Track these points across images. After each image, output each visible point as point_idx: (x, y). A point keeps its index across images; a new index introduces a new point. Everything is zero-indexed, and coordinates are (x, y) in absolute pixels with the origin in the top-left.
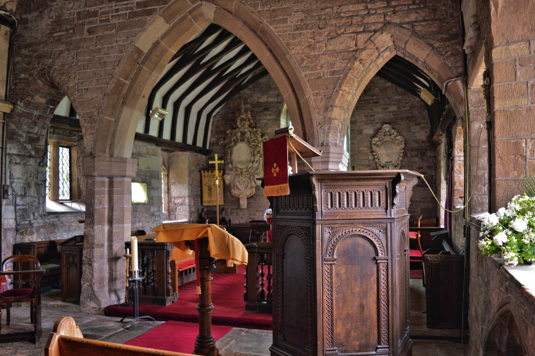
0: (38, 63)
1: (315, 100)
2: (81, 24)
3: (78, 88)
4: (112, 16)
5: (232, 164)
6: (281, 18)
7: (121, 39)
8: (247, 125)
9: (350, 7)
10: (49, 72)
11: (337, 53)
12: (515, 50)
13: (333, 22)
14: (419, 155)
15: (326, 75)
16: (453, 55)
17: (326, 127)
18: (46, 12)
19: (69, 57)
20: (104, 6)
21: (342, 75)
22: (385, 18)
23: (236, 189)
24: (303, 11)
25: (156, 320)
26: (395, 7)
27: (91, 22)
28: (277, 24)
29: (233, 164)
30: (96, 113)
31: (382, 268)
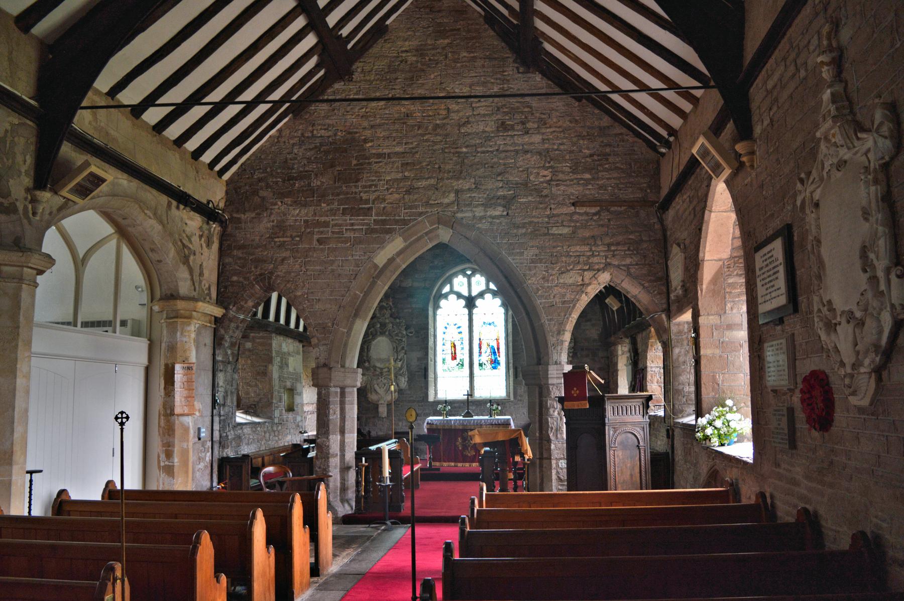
0: (256, 267)
1: (549, 324)
2: (309, 233)
3: (307, 297)
4: (346, 229)
5: (369, 362)
6: (518, 251)
7: (358, 253)
8: (387, 315)
9: (578, 248)
10: (270, 278)
11: (567, 286)
12: (712, 319)
13: (564, 259)
14: (590, 355)
15: (558, 303)
16: (659, 294)
17: (559, 348)
18: (265, 215)
19: (295, 265)
20: (337, 218)
21: (571, 305)
22: (606, 259)
23: (373, 393)
24: (537, 247)
25: (402, 524)
26: (614, 251)
27: (322, 233)
28: (515, 256)
29: (371, 362)
30: (330, 324)
31: (642, 452)
